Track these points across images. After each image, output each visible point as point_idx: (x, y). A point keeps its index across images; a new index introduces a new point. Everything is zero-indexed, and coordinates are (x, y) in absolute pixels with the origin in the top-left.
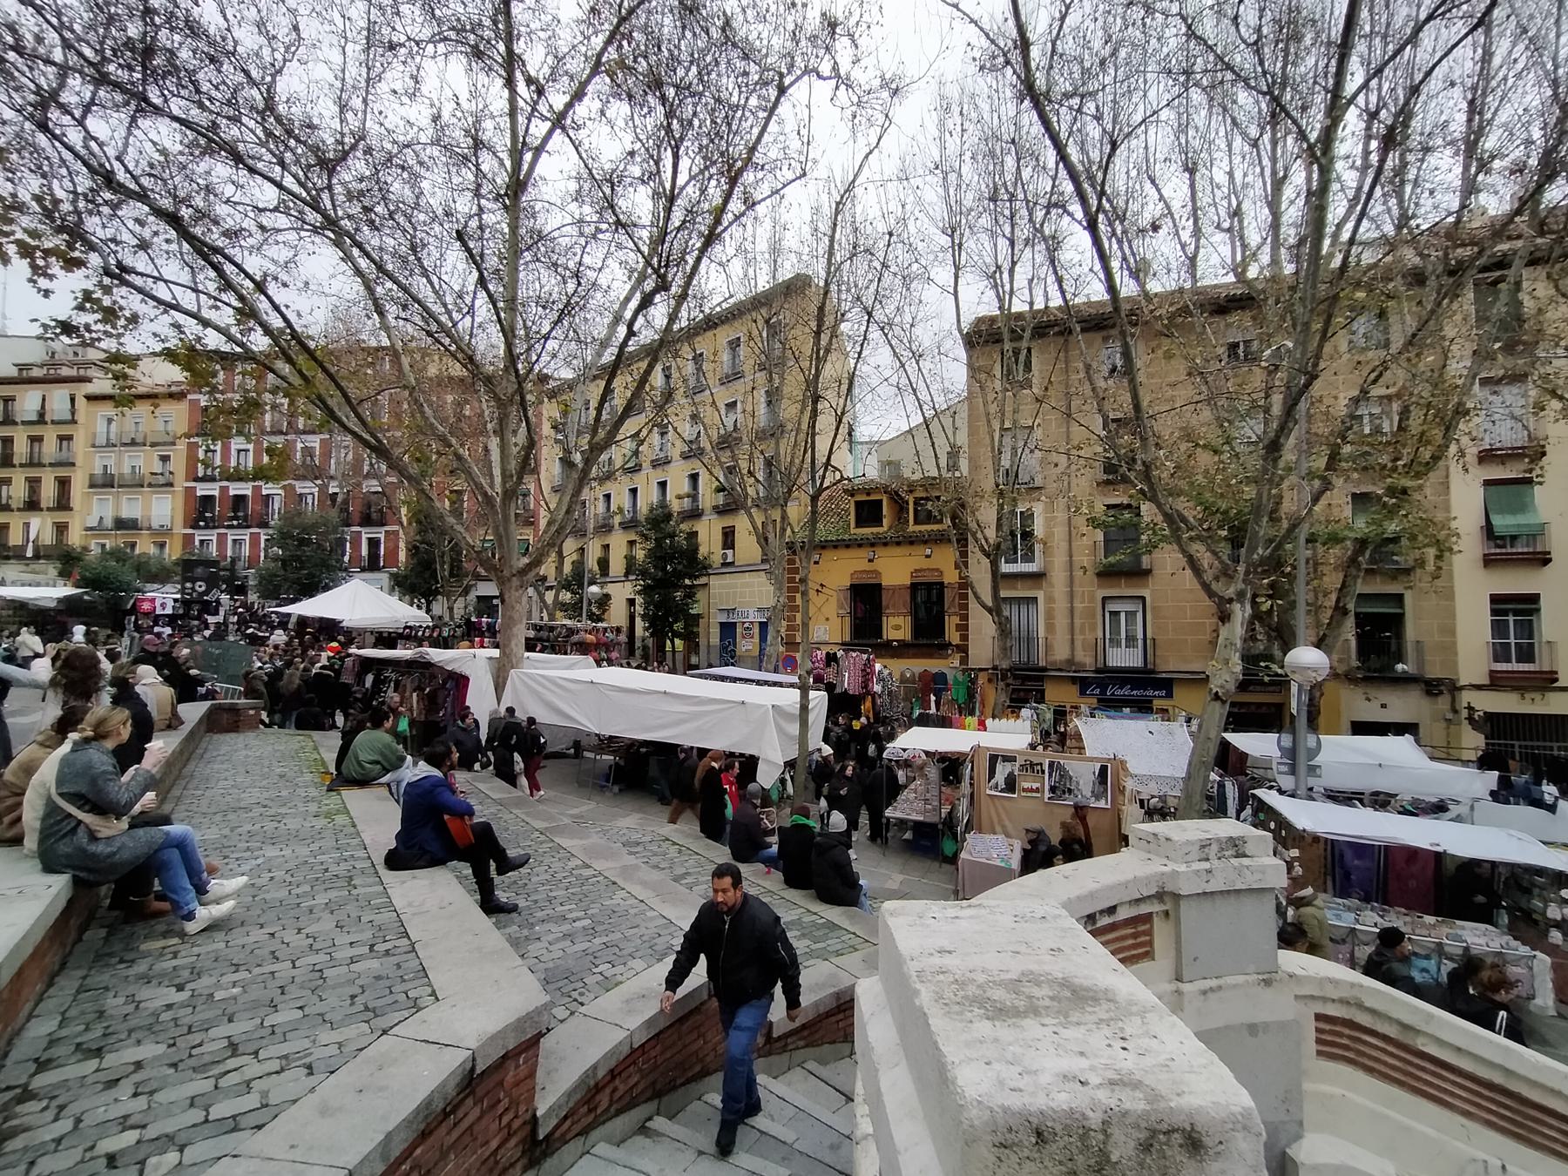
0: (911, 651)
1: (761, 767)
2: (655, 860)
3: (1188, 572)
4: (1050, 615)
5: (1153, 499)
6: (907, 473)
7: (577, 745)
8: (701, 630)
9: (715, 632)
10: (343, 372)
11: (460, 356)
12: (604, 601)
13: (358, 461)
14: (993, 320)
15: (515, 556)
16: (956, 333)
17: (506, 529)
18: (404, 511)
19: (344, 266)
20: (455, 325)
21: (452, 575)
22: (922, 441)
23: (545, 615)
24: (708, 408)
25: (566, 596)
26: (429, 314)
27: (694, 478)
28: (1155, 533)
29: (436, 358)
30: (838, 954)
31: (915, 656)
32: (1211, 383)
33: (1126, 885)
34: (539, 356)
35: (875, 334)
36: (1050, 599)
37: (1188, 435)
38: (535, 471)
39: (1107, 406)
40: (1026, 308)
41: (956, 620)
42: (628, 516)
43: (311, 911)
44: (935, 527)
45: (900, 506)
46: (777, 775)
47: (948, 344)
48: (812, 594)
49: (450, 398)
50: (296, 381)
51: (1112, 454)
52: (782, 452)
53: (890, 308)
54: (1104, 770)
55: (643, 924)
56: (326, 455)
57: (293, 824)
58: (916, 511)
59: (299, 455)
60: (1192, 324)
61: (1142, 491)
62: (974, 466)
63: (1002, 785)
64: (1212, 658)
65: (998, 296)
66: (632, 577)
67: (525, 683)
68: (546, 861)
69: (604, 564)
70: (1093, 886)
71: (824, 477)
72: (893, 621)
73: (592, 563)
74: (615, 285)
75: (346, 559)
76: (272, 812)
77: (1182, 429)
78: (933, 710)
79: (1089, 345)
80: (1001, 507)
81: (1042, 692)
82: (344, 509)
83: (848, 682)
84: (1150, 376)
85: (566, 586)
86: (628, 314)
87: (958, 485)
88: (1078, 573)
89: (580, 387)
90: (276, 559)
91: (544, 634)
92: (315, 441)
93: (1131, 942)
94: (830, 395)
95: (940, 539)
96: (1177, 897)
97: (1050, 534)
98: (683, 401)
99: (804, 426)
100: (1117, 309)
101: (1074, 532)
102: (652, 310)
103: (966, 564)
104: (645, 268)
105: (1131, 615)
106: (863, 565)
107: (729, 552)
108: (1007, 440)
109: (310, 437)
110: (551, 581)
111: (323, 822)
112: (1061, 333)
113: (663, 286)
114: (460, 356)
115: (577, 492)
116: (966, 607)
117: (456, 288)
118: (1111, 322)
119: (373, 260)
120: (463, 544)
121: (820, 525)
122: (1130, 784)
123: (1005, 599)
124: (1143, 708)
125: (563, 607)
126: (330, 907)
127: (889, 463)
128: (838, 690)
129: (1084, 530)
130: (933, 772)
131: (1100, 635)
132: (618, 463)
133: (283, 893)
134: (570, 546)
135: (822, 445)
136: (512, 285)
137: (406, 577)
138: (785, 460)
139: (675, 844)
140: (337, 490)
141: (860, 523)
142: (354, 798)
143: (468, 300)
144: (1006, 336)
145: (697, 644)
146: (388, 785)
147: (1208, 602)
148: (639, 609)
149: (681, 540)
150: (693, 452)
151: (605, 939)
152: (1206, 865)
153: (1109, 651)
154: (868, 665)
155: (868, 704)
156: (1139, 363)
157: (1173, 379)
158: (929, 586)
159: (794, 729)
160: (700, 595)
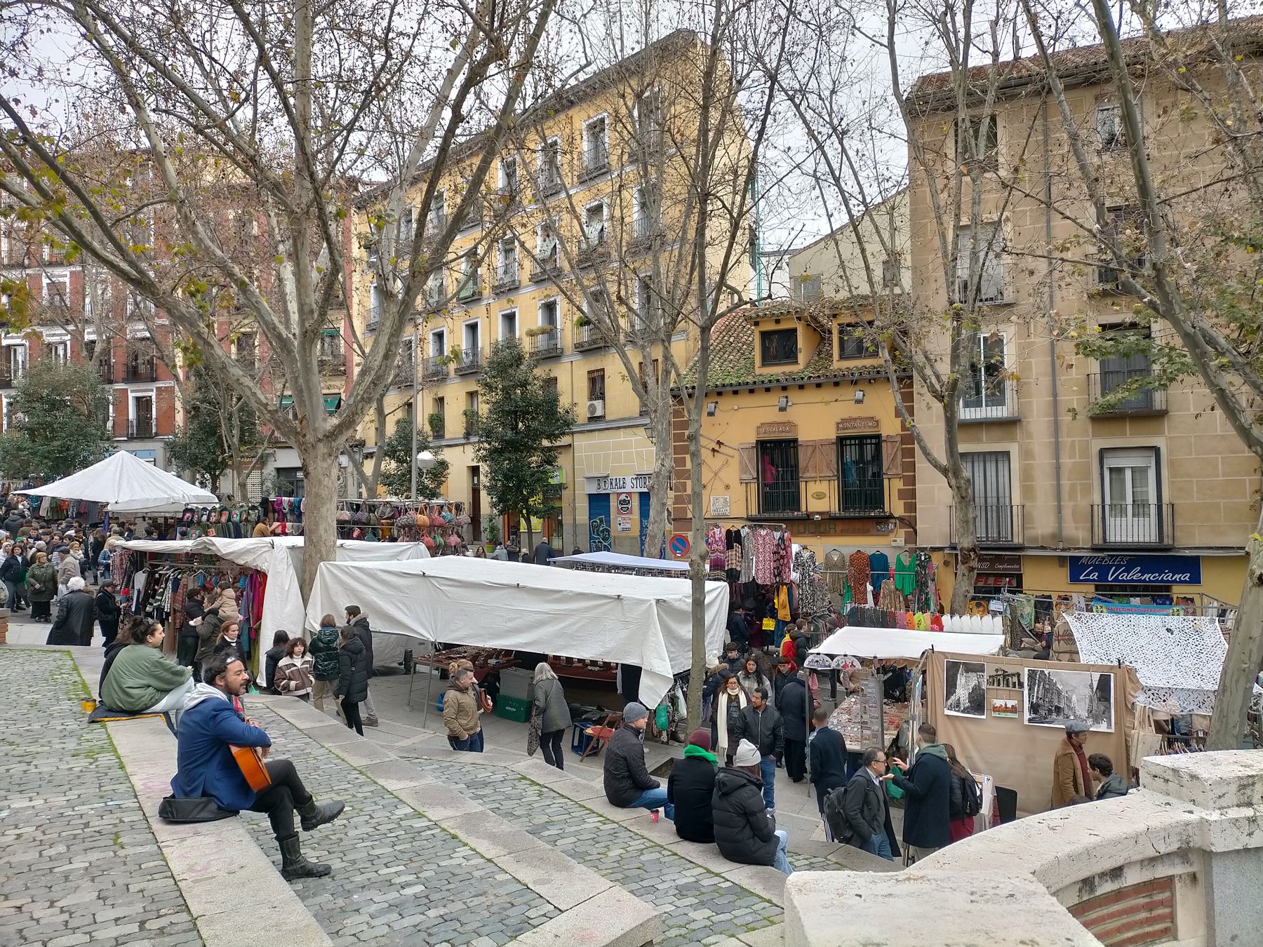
0: (840, 527)
1: (644, 681)
2: (508, 805)
3: (1219, 412)
4: (1027, 475)
5: (1169, 315)
6: (828, 292)
7: (408, 656)
8: (565, 504)
9: (583, 506)
10: (95, 185)
11: (239, 158)
12: (439, 472)
13: (120, 300)
14: (942, 79)
15: (321, 415)
16: (892, 100)
17: (307, 381)
18: (179, 360)
19: (86, 45)
20: (232, 115)
21: (242, 441)
22: (848, 247)
23: (363, 490)
24: (566, 217)
25: (390, 466)
26: (200, 107)
27: (550, 308)
28: (1171, 360)
29: (211, 161)
30: (749, 928)
31: (844, 533)
32: (1249, 152)
33: (1136, 839)
34: (341, 152)
35: (782, 105)
36: (1027, 454)
37: (1216, 224)
38: (345, 305)
39: (1102, 189)
40: (988, 60)
41: (898, 484)
42: (467, 360)
43: (67, 878)
44: (868, 362)
45: (820, 334)
46: (664, 691)
47: (881, 116)
48: (705, 454)
49: (231, 214)
50: (35, 198)
51: (1109, 256)
52: (663, 270)
53: (803, 68)
54: (1104, 683)
55: (491, 891)
56: (80, 293)
57: (45, 765)
58: (842, 343)
59: (45, 291)
60: (1222, 70)
61: (1152, 305)
62: (920, 278)
63: (965, 702)
64: (1254, 528)
65: (949, 45)
66: (474, 439)
67: (340, 582)
68: (368, 808)
69: (437, 423)
70: (1087, 841)
71: (716, 302)
72: (813, 488)
73: (421, 420)
74: (436, 54)
75: (110, 424)
76: (20, 751)
77: (1207, 217)
78: (870, 603)
79: (1075, 108)
80: (957, 331)
81: (1019, 578)
82: (105, 362)
83: (758, 569)
84: (1161, 146)
85: (391, 453)
86: (454, 94)
87: (897, 304)
88: (1066, 418)
89: (396, 193)
90: (20, 428)
91: (363, 515)
92: (64, 275)
93: (1143, 915)
94: (725, 193)
95: (875, 378)
96: (1207, 855)
97: (1024, 366)
98: (531, 208)
99: (691, 234)
100: (1113, 56)
101: (1058, 363)
102: (486, 86)
103: (911, 411)
104: (474, 33)
105: (1138, 472)
106: (772, 415)
107: (598, 403)
108: (966, 243)
109: (57, 271)
110: (371, 446)
111: (82, 763)
112: (1037, 93)
113: (498, 53)
114: (239, 158)
115: (397, 331)
116: (912, 467)
117: (232, 68)
118: (1105, 74)
119: (122, 36)
120: (254, 405)
121: (715, 365)
122: (1141, 700)
123: (963, 455)
124: (1159, 597)
125: (388, 480)
126: (91, 873)
127: (805, 279)
128: (743, 579)
129: (1073, 359)
130: (873, 687)
131: (1097, 499)
132: (451, 289)
133: (32, 855)
134: (393, 400)
135: (714, 258)
136: (303, 60)
137: (184, 446)
138: (666, 281)
139: (533, 783)
140: (93, 337)
141: (767, 360)
142: (123, 732)
143: (246, 82)
144: (961, 101)
145: (560, 523)
146: (166, 714)
147: (1248, 453)
148: (484, 480)
149: (536, 389)
150: (546, 274)
151: (442, 911)
152: (1249, 812)
153: (1110, 521)
154: (783, 545)
155: (783, 596)
156: (1146, 130)
157: (1192, 148)
158: (861, 440)
159: (686, 631)
160: (563, 460)
